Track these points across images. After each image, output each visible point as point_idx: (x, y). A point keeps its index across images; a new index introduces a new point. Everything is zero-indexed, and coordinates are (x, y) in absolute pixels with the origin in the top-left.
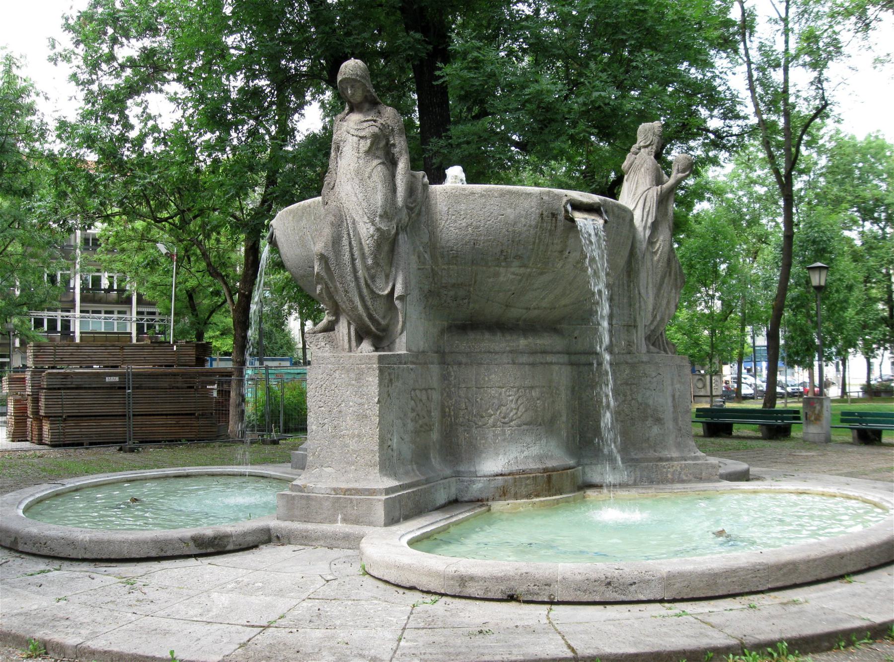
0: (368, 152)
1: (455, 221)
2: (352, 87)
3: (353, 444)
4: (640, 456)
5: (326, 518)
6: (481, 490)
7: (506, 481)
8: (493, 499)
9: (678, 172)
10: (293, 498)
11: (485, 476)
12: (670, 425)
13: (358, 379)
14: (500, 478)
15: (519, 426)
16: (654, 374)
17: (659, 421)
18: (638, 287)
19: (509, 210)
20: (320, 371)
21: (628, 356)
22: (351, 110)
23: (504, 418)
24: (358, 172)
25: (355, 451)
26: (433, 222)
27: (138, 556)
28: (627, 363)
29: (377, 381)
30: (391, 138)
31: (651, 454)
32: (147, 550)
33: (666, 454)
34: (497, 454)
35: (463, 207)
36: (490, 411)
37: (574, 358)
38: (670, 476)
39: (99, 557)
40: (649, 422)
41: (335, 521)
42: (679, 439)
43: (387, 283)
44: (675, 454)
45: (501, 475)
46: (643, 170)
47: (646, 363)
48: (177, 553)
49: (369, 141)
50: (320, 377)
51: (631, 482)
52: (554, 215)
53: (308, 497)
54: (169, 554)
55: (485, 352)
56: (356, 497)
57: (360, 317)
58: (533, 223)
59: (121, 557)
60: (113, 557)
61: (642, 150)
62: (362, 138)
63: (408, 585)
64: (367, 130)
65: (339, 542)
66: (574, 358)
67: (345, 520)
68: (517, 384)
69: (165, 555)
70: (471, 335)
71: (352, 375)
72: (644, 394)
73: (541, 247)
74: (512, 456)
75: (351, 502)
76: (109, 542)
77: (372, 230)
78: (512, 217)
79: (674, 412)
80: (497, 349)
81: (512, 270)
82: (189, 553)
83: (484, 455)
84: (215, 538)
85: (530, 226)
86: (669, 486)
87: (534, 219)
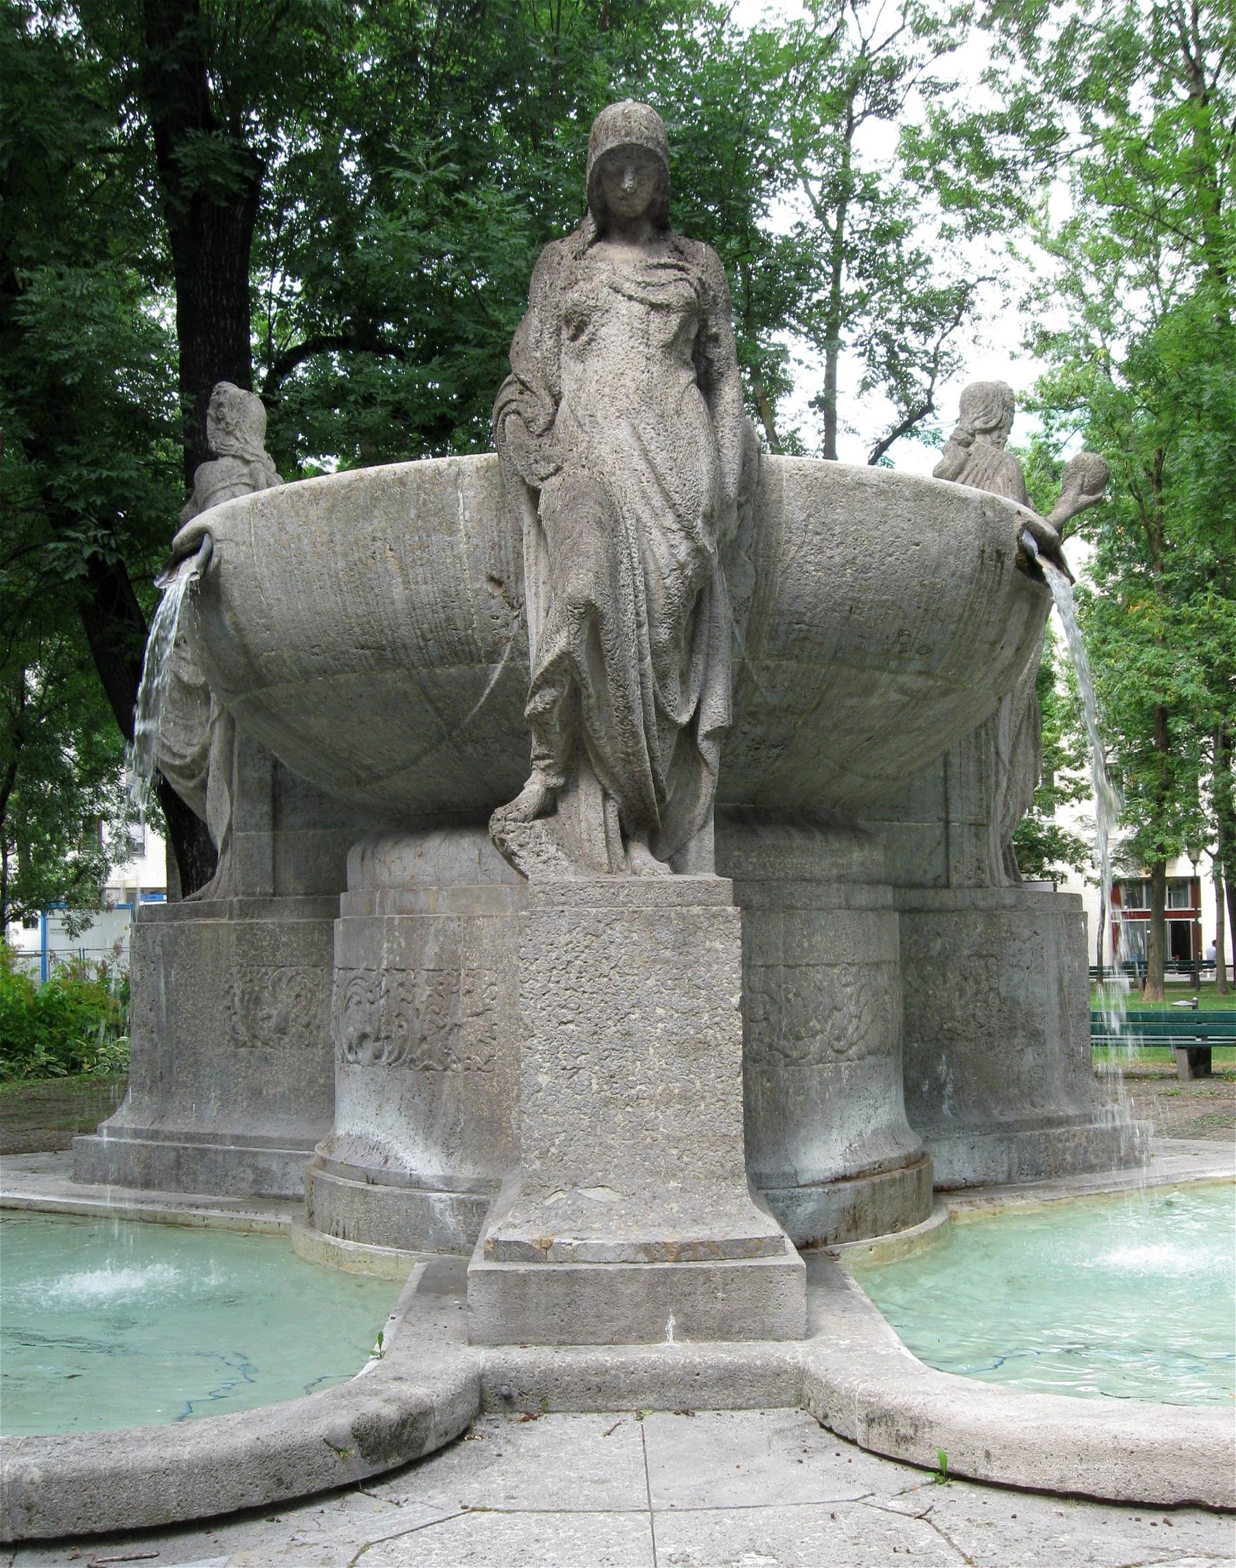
0: (669, 347)
1: (821, 551)
2: (637, 171)
3: (667, 1122)
4: (1010, 1117)
5: (629, 1330)
6: (812, 1219)
7: (859, 1193)
8: (837, 1239)
9: (1082, 491)
10: (524, 1279)
11: (814, 1184)
12: (1054, 1045)
13: (681, 946)
14: (848, 1185)
15: (861, 1058)
16: (1026, 933)
17: (1035, 1036)
18: (996, 738)
19: (930, 535)
20: (564, 924)
21: (979, 894)
22: (602, 235)
23: (838, 1039)
24: (648, 396)
25: (671, 1140)
26: (769, 546)
27: (211, 1512)
28: (976, 908)
29: (736, 949)
30: (712, 321)
31: (1028, 1112)
32: (239, 1489)
33: (1051, 1109)
34: (829, 1128)
35: (840, 515)
36: (814, 1023)
37: (914, 898)
38: (1069, 1158)
39: (81, 1528)
40: (1019, 1041)
41: (656, 1336)
42: (1071, 1076)
43: (685, 692)
44: (1071, 1111)
45: (845, 1178)
46: (999, 480)
47: (1013, 908)
48: (318, 1485)
49: (675, 320)
50: (564, 939)
51: (1001, 1177)
52: (1000, 555)
53: (569, 1274)
54: (298, 1490)
55: (795, 880)
56: (720, 1264)
57: (640, 785)
58: (968, 570)
59: (159, 1519)
60: (129, 1524)
61: (979, 438)
62: (655, 307)
63: (1171, 1498)
64: (672, 288)
65: (705, 1394)
66: (914, 898)
67: (687, 1331)
68: (858, 958)
69: (289, 1494)
70: (768, 838)
71: (664, 935)
72: (1010, 979)
73: (970, 627)
74: (853, 1133)
75: (708, 1280)
76: (117, 1477)
77: (683, 550)
78: (934, 550)
79: (1062, 1017)
80: (817, 872)
81: (903, 679)
82: (347, 1479)
83: (803, 1132)
84: (403, 1423)
85: (961, 577)
86: (1069, 1180)
87: (967, 563)
